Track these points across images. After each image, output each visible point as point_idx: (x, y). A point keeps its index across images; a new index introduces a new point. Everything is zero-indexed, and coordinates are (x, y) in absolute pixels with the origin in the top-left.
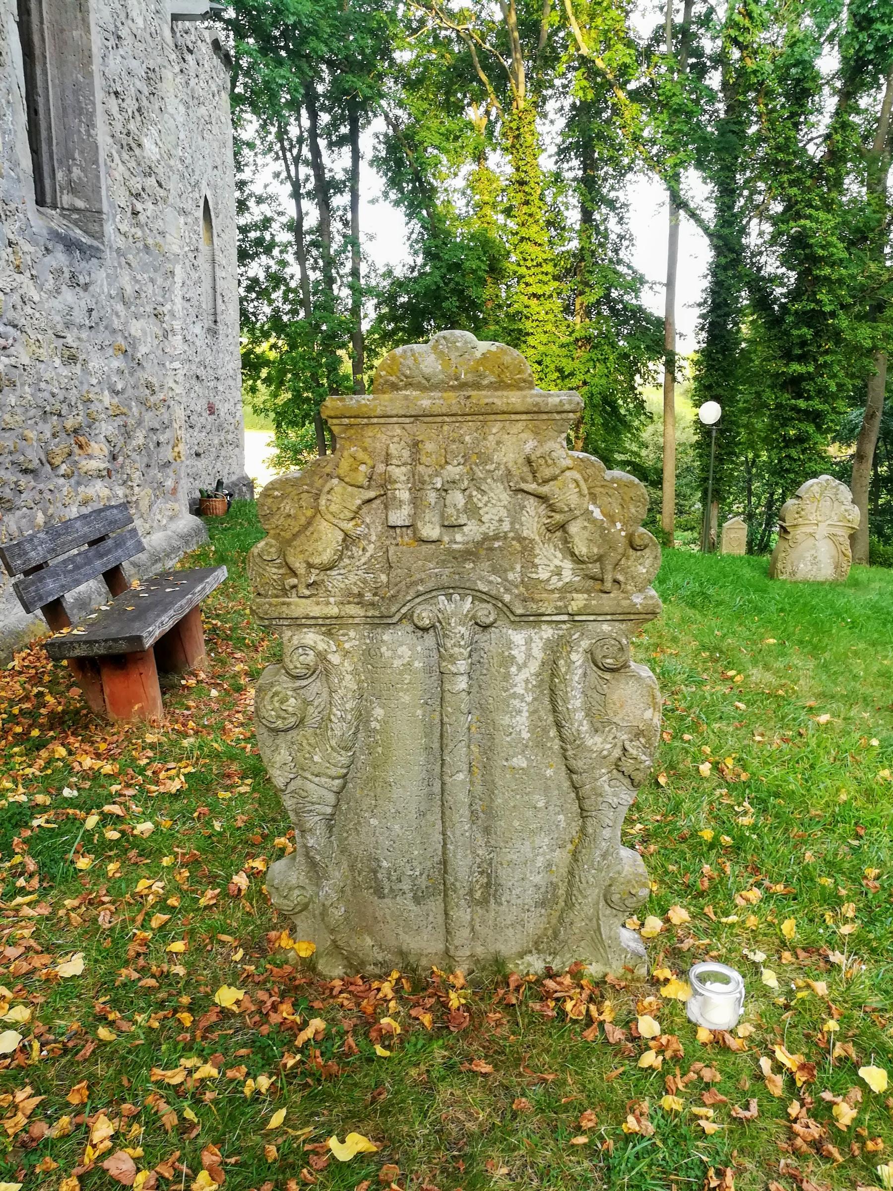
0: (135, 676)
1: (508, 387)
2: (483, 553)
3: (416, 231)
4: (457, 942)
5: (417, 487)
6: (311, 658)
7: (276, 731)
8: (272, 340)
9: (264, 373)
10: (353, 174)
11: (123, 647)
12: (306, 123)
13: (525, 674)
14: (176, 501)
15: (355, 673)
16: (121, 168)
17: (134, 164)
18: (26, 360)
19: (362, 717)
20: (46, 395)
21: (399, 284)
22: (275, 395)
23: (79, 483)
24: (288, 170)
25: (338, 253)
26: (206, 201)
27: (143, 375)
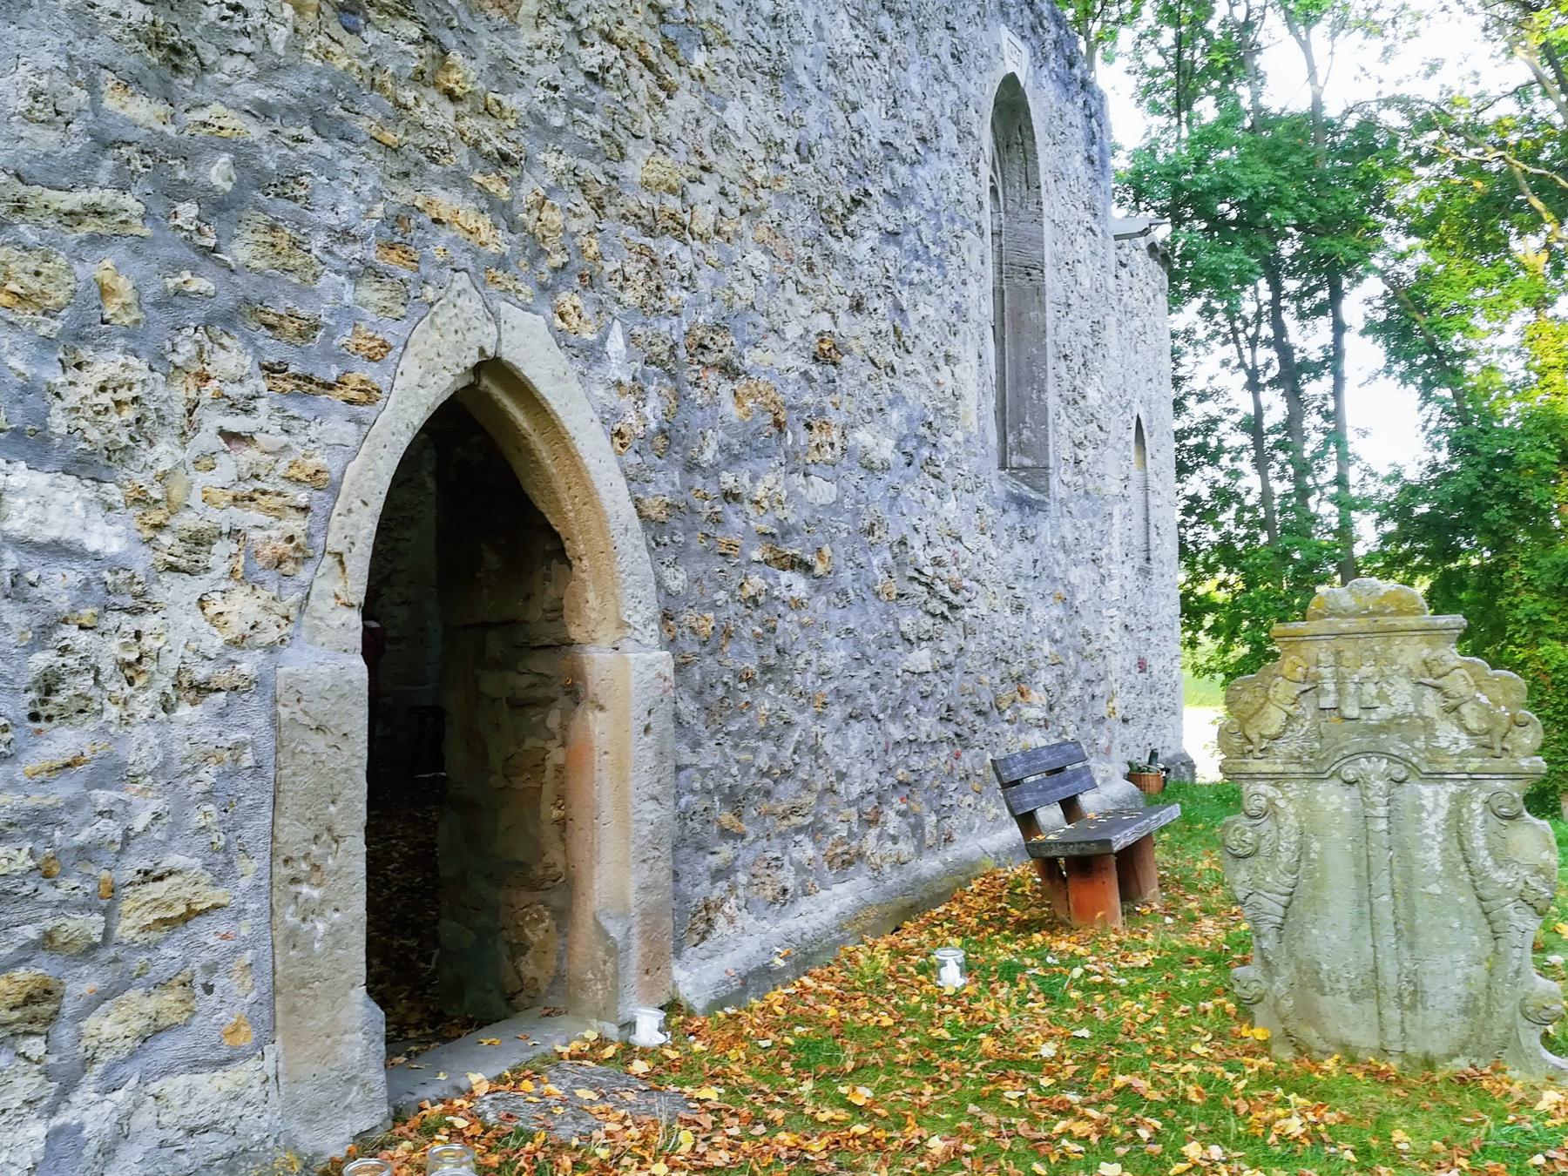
0: (1099, 884)
1: (1406, 613)
2: (1393, 727)
3: (1436, 417)
4: (1389, 1038)
5: (1340, 681)
6: (1263, 802)
7: (1238, 857)
8: (1221, 575)
9: (1208, 620)
10: (1334, 358)
11: (1094, 849)
12: (1266, 294)
13: (1434, 819)
14: (1110, 762)
15: (1297, 815)
16: (1068, 422)
17: (1078, 415)
18: (984, 611)
19: (1303, 849)
20: (998, 642)
21: (1413, 492)
22: (1225, 651)
23: (1020, 731)
24: (1241, 355)
25: (1318, 455)
26: (1139, 420)
27: (1081, 624)
